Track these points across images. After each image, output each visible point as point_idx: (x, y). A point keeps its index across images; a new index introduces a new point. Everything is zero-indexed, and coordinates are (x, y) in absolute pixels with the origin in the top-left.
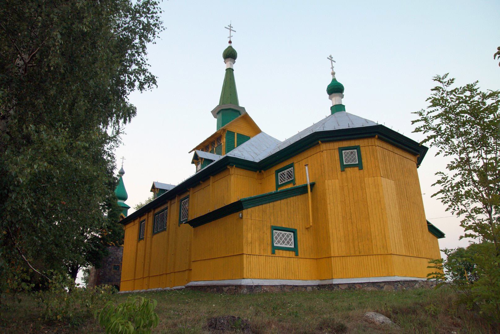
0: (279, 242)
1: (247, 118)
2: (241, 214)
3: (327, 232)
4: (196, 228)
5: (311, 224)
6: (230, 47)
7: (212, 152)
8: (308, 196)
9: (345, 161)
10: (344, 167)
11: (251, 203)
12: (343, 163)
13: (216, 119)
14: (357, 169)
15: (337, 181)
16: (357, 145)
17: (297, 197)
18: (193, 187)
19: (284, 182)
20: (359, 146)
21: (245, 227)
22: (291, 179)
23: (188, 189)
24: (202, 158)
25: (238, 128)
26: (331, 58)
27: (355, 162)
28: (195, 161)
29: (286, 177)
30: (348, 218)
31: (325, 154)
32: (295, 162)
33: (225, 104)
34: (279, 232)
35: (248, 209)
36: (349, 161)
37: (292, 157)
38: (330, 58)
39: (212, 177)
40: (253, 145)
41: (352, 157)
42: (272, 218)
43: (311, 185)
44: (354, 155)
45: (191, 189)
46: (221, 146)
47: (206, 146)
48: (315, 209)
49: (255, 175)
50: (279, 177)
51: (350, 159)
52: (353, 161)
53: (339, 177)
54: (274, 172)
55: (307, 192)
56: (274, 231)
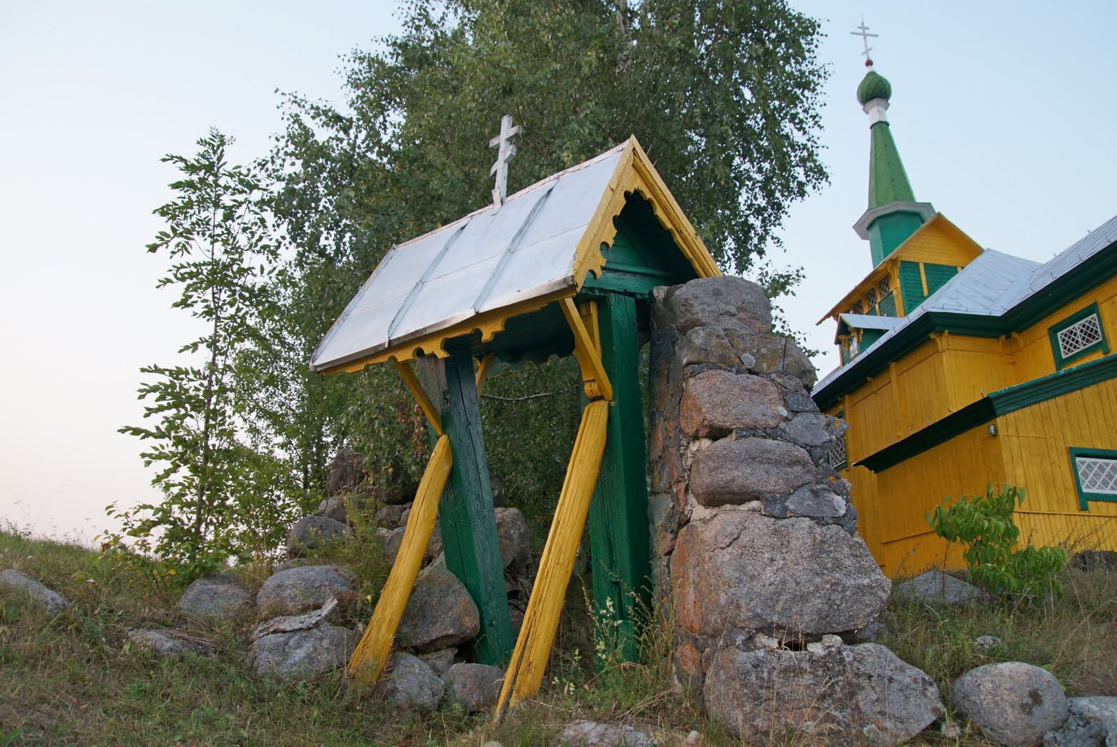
1: (941, 226)
2: (992, 428)
4: (883, 473)
7: (872, 312)
11: (1012, 401)
13: (868, 242)
18: (851, 393)
21: (1005, 455)
23: (839, 399)
24: (858, 330)
25: (925, 252)
28: (842, 337)
33: (883, 205)
35: (1008, 415)
40: (976, 282)
45: (847, 396)
46: (893, 298)
47: (857, 300)
49: (997, 345)
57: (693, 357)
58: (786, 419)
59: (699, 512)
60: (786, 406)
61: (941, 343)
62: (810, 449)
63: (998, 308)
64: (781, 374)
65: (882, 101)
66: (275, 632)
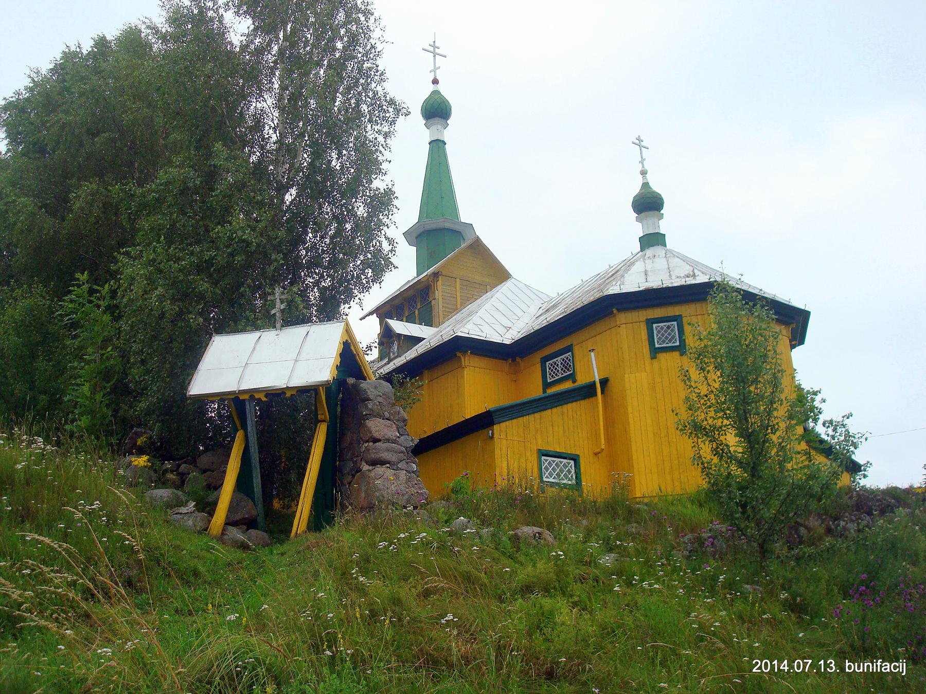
0: (551, 474)
1: (478, 249)
2: (490, 432)
3: (630, 459)
5: (603, 447)
6: (436, 93)
8: (597, 400)
9: (658, 342)
10: (655, 352)
12: (654, 345)
14: (676, 354)
15: (644, 375)
16: (677, 314)
17: (578, 402)
19: (557, 378)
20: (680, 316)
21: (497, 451)
22: (569, 373)
24: (399, 335)
26: (639, 143)
27: (674, 343)
29: (560, 370)
30: (663, 435)
31: (623, 330)
32: (575, 343)
34: (550, 459)
36: (664, 342)
37: (569, 334)
38: (638, 142)
39: (426, 371)
41: (669, 334)
42: (539, 437)
43: (601, 383)
44: (673, 331)
48: (610, 423)
49: (505, 365)
50: (548, 370)
51: (667, 338)
52: (670, 341)
53: (648, 368)
54: (539, 360)
55: (596, 395)
56: (543, 458)
57: (368, 413)
58: (399, 437)
59: (365, 467)
60: (399, 432)
61: (465, 358)
62: (406, 448)
63: (507, 338)
64: (398, 420)
65: (442, 121)
66: (176, 514)
